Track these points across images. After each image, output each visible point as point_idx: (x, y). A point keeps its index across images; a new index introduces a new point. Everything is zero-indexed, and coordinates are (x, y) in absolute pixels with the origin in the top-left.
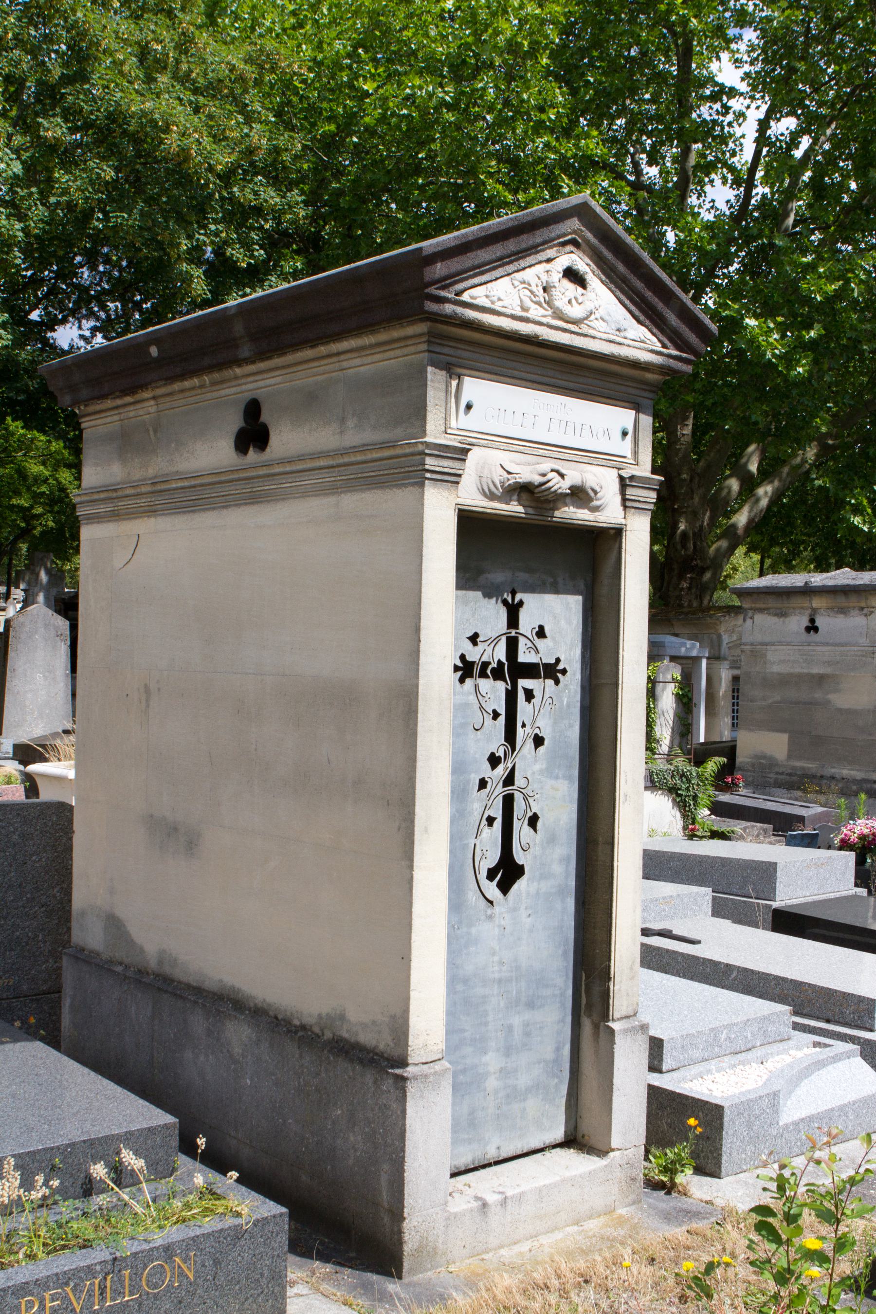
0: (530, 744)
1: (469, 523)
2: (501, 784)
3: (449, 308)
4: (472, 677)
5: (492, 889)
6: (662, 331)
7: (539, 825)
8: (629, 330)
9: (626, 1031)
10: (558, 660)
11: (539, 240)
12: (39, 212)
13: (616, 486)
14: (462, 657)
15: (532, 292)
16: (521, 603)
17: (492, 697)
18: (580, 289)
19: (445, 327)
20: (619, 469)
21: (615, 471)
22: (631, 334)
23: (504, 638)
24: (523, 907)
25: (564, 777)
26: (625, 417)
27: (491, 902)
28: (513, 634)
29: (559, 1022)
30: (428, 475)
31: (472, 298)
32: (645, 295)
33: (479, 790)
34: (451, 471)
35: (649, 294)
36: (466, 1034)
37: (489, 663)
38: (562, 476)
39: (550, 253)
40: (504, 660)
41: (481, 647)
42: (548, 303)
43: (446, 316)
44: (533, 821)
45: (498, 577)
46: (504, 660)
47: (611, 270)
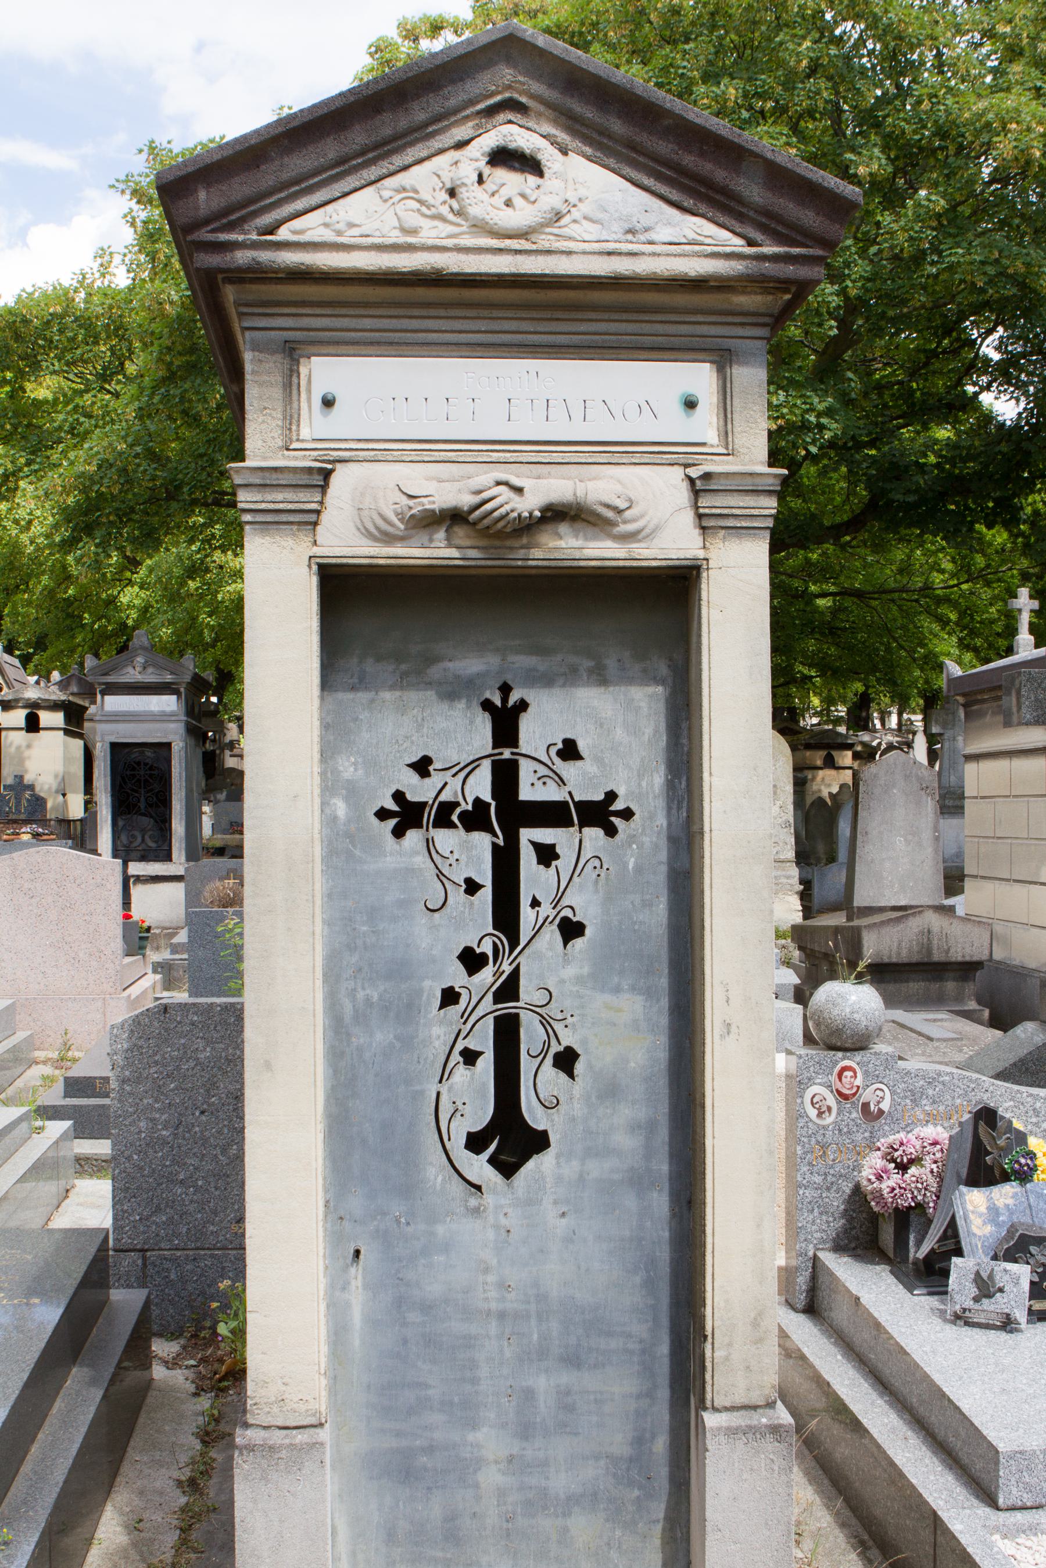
0: (552, 935)
1: (343, 589)
2: (490, 997)
3: (242, 257)
4: (419, 826)
5: (479, 1167)
6: (741, 217)
7: (579, 1067)
9: (732, 1432)
10: (611, 796)
11: (421, 116)
12: (861, 268)
14: (399, 796)
16: (523, 706)
17: (463, 859)
18: (532, 180)
20: (686, 466)
21: (678, 472)
22: (663, 234)
23: (487, 764)
24: (547, 1201)
25: (633, 988)
26: (699, 377)
27: (479, 1188)
28: (507, 754)
29: (639, 1397)
30: (247, 517)
31: (295, 232)
32: (682, 161)
33: (442, 1006)
34: (290, 506)
35: (689, 160)
36: (430, 1392)
37: (457, 804)
38: (519, 490)
39: (460, 133)
40: (487, 796)
41: (436, 780)
42: (460, 213)
43: (239, 270)
44: (566, 1061)
45: (471, 664)
46: (487, 796)
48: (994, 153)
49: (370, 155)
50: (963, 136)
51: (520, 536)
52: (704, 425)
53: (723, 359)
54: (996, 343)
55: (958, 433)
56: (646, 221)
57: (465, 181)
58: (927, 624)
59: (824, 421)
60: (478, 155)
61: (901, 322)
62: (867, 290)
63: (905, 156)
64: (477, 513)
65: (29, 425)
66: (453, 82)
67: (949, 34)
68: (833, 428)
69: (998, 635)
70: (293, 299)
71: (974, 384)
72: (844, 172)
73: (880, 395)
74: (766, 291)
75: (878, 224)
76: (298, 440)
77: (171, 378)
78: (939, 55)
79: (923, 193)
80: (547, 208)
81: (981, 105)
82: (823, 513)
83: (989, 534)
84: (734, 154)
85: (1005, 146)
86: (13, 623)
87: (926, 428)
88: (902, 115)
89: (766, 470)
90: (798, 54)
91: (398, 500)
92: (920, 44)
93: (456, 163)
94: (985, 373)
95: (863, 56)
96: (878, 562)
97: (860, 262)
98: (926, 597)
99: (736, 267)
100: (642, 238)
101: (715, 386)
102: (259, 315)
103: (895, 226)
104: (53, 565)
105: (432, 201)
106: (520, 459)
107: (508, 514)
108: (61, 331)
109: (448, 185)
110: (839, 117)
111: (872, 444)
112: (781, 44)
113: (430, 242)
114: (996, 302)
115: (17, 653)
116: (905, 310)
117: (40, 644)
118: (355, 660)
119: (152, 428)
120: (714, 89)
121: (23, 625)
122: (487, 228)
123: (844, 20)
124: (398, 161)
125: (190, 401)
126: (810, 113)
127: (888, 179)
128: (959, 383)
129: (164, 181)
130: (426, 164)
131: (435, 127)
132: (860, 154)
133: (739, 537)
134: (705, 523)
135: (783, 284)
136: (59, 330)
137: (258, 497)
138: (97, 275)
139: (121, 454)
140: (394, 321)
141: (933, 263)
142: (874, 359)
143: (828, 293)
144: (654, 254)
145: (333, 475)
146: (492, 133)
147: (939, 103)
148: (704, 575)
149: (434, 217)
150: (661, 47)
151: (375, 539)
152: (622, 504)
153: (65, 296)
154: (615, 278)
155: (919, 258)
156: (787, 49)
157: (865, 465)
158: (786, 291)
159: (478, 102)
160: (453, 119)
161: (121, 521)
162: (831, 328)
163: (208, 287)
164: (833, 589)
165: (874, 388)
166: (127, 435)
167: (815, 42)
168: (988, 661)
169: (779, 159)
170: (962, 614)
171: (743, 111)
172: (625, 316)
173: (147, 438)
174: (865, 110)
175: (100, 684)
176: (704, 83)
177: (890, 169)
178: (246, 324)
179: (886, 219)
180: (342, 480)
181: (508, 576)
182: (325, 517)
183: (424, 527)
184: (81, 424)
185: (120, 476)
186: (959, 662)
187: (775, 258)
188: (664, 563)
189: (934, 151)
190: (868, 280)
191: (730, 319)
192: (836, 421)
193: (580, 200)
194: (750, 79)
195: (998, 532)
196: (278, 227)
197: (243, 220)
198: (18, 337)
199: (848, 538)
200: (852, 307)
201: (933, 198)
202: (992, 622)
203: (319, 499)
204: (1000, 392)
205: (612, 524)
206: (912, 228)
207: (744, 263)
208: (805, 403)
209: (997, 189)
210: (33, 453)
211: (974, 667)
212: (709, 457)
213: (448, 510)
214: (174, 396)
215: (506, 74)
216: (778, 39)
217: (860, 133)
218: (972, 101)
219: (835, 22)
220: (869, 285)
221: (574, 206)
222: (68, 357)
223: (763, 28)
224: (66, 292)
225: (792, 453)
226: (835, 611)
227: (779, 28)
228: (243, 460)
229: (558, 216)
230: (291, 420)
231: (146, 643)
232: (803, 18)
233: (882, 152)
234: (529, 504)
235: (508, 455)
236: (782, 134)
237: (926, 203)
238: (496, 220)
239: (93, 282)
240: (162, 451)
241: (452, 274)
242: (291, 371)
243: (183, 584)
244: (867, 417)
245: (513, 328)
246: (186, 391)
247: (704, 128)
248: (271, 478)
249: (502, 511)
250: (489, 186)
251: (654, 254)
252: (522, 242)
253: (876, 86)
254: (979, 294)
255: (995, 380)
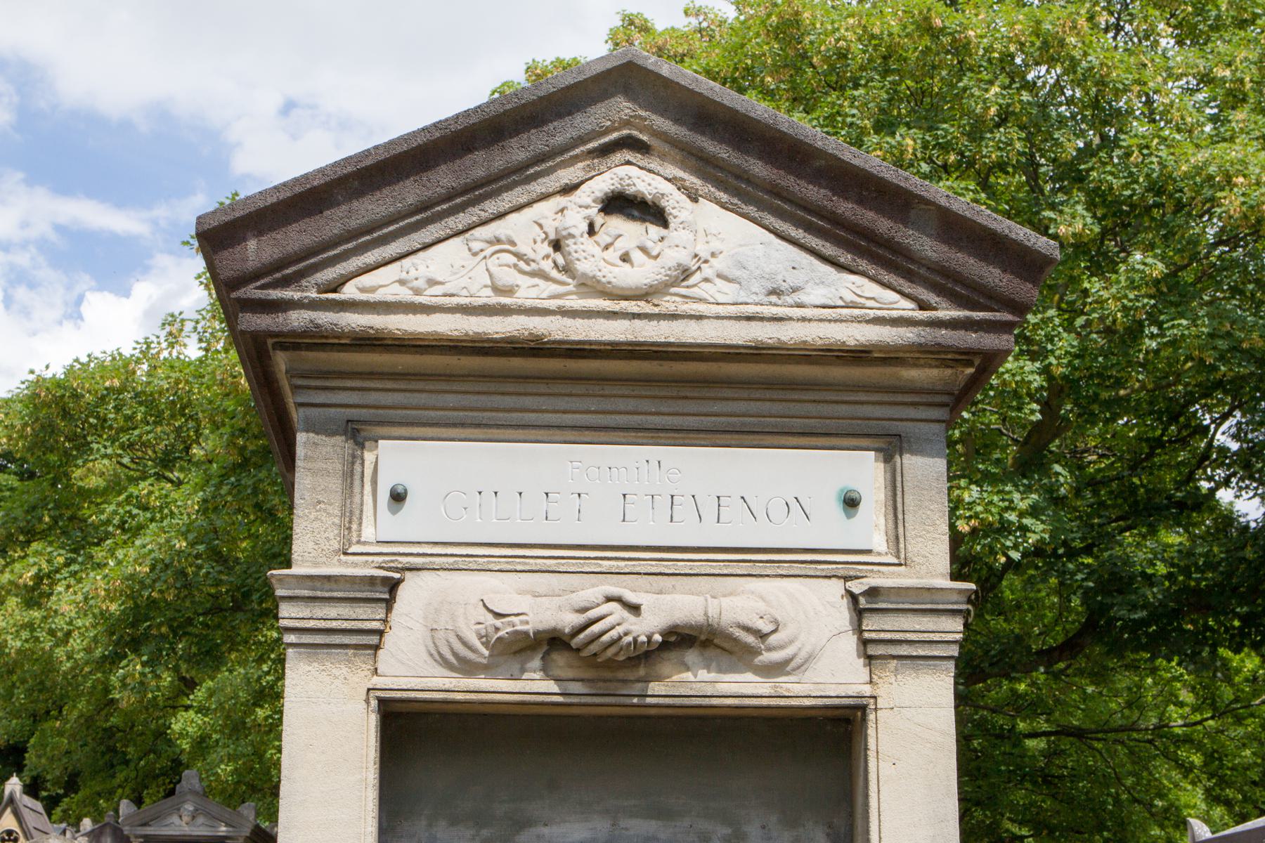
1: (408, 731)
3: (297, 319)
6: (910, 276)
8: (808, 289)
12: (1066, 342)
13: (843, 615)
15: (519, 256)
18: (655, 231)
19: (322, 355)
20: (847, 579)
21: (837, 587)
22: (815, 295)
26: (862, 469)
30: (290, 638)
31: (362, 290)
32: (838, 209)
34: (346, 625)
35: (846, 208)
38: (635, 609)
42: (567, 269)
43: (293, 333)
47: (738, 177)
48: (1218, 210)
49: (458, 201)
50: (1181, 191)
51: (637, 666)
52: (870, 529)
53: (891, 446)
54: (1234, 430)
55: (1193, 538)
56: (793, 279)
57: (573, 231)
58: (1164, 772)
59: (1027, 521)
60: (589, 201)
61: (1117, 406)
62: (1075, 369)
63: (1114, 215)
64: (582, 636)
65: (71, 519)
66: (560, 116)
67: (1159, 79)
68: (1038, 530)
69: (1254, 783)
70: (360, 370)
71: (1210, 479)
72: (1042, 228)
73: (1095, 493)
74: (944, 364)
75: (1086, 293)
76: (359, 542)
77: (242, 466)
78: (1149, 102)
79: (1138, 256)
80: (673, 263)
81: (1201, 156)
82: (1029, 635)
83: (1236, 660)
84: (898, 202)
85: (1231, 203)
86: (39, 757)
87: (1153, 531)
88: (1108, 168)
89: (947, 583)
90: (984, 101)
91: (481, 619)
92: (1126, 90)
93: (562, 210)
94: (1222, 465)
95: (1061, 104)
96: (1101, 693)
97: (1065, 335)
98: (1161, 737)
99: (907, 335)
100: (789, 300)
101: (881, 480)
102: (317, 388)
103: (1105, 294)
104: (94, 687)
105: (531, 255)
106: (637, 569)
107: (620, 638)
108: (118, 409)
109: (552, 236)
110: (1036, 171)
111: (1088, 550)
112: (965, 89)
113: (528, 303)
114: (1230, 382)
115: (44, 794)
116: (1122, 392)
117: (71, 784)
118: (424, 823)
119: (218, 523)
120: (888, 139)
121: (51, 760)
122: (600, 288)
123: (1037, 64)
124: (491, 207)
125: (265, 493)
126: (1001, 166)
127: (1094, 240)
128: (1190, 478)
129: (206, 227)
130: (526, 211)
131: (537, 169)
132: (1061, 212)
133: (916, 669)
134: (871, 652)
135: (964, 356)
136: (114, 408)
137: (306, 613)
138: (164, 345)
139: (180, 552)
140: (484, 398)
141: (1152, 336)
142: (1087, 451)
143: (1020, 370)
144: (804, 319)
145: (401, 587)
146: (607, 176)
147: (1151, 154)
148: (872, 717)
149: (533, 274)
150: (826, 93)
151: (451, 667)
152: (766, 627)
153: (123, 366)
154: (756, 348)
155: (1135, 332)
156: (972, 95)
157: (1079, 577)
158: (969, 363)
159: (590, 140)
160: (558, 160)
161: (175, 635)
162: (1033, 412)
163: (256, 351)
164: (1045, 727)
165: (1088, 485)
166: (188, 531)
167: (1004, 88)
168: (1244, 818)
169: (955, 207)
170: (1210, 757)
171: (923, 164)
172: (768, 394)
173: (212, 535)
174: (1065, 164)
175: (137, 837)
176: (876, 133)
177: (1097, 229)
178: (300, 400)
179: (1094, 285)
180: (412, 593)
181: (620, 717)
182: (388, 639)
183: (515, 653)
184: (133, 517)
185: (176, 580)
186: (1207, 820)
187: (953, 324)
188: (820, 702)
189: (1148, 209)
190: (1076, 356)
191: (900, 398)
192: (1043, 522)
193: (713, 255)
194: (930, 129)
195: (1248, 655)
196: (344, 284)
197: (301, 275)
198: (66, 414)
199: (1061, 665)
200: (1058, 389)
201: (1150, 261)
202: (1247, 768)
203: (382, 616)
204: (1240, 489)
205: (755, 652)
206: (1126, 296)
207: (915, 330)
208: (1003, 500)
209: (1223, 253)
210: (75, 551)
211: (1226, 826)
212: (876, 568)
213: (544, 631)
214: (246, 487)
215: (622, 107)
216: (961, 84)
217: (1060, 189)
218: (1190, 152)
219: (1027, 65)
220: (1076, 362)
221: (706, 261)
222: (124, 438)
223: (944, 73)
224: (127, 362)
225: (990, 560)
226: (1050, 754)
227: (961, 74)
228: (289, 566)
229: (686, 273)
230: (350, 518)
231: (197, 786)
232: (990, 61)
233: (1087, 209)
234: (647, 626)
235: (622, 564)
236: (967, 189)
237: (1142, 267)
238: (610, 277)
239: (158, 353)
240: (230, 550)
241: (554, 342)
242: (354, 456)
243: (249, 711)
244: (1080, 518)
245: (630, 408)
246: (261, 481)
247: (863, 170)
248: (323, 589)
249: (613, 634)
250: (603, 237)
251: (804, 319)
252: (642, 303)
253: (1078, 137)
254: (1209, 372)
255: (1234, 474)
